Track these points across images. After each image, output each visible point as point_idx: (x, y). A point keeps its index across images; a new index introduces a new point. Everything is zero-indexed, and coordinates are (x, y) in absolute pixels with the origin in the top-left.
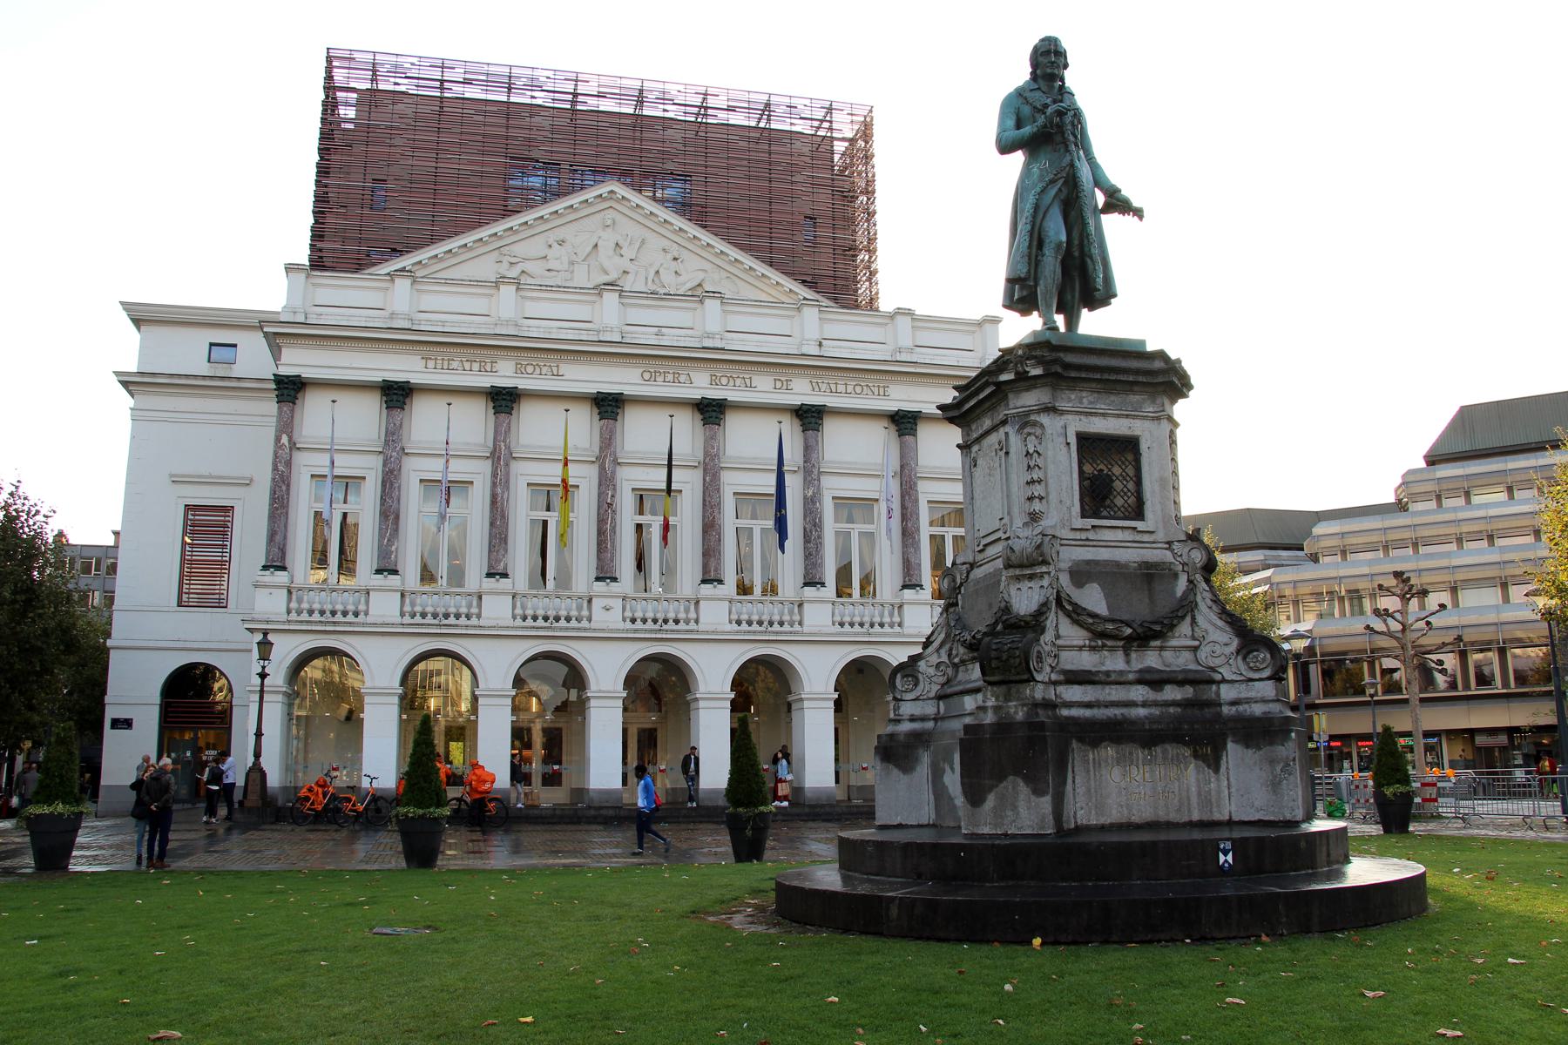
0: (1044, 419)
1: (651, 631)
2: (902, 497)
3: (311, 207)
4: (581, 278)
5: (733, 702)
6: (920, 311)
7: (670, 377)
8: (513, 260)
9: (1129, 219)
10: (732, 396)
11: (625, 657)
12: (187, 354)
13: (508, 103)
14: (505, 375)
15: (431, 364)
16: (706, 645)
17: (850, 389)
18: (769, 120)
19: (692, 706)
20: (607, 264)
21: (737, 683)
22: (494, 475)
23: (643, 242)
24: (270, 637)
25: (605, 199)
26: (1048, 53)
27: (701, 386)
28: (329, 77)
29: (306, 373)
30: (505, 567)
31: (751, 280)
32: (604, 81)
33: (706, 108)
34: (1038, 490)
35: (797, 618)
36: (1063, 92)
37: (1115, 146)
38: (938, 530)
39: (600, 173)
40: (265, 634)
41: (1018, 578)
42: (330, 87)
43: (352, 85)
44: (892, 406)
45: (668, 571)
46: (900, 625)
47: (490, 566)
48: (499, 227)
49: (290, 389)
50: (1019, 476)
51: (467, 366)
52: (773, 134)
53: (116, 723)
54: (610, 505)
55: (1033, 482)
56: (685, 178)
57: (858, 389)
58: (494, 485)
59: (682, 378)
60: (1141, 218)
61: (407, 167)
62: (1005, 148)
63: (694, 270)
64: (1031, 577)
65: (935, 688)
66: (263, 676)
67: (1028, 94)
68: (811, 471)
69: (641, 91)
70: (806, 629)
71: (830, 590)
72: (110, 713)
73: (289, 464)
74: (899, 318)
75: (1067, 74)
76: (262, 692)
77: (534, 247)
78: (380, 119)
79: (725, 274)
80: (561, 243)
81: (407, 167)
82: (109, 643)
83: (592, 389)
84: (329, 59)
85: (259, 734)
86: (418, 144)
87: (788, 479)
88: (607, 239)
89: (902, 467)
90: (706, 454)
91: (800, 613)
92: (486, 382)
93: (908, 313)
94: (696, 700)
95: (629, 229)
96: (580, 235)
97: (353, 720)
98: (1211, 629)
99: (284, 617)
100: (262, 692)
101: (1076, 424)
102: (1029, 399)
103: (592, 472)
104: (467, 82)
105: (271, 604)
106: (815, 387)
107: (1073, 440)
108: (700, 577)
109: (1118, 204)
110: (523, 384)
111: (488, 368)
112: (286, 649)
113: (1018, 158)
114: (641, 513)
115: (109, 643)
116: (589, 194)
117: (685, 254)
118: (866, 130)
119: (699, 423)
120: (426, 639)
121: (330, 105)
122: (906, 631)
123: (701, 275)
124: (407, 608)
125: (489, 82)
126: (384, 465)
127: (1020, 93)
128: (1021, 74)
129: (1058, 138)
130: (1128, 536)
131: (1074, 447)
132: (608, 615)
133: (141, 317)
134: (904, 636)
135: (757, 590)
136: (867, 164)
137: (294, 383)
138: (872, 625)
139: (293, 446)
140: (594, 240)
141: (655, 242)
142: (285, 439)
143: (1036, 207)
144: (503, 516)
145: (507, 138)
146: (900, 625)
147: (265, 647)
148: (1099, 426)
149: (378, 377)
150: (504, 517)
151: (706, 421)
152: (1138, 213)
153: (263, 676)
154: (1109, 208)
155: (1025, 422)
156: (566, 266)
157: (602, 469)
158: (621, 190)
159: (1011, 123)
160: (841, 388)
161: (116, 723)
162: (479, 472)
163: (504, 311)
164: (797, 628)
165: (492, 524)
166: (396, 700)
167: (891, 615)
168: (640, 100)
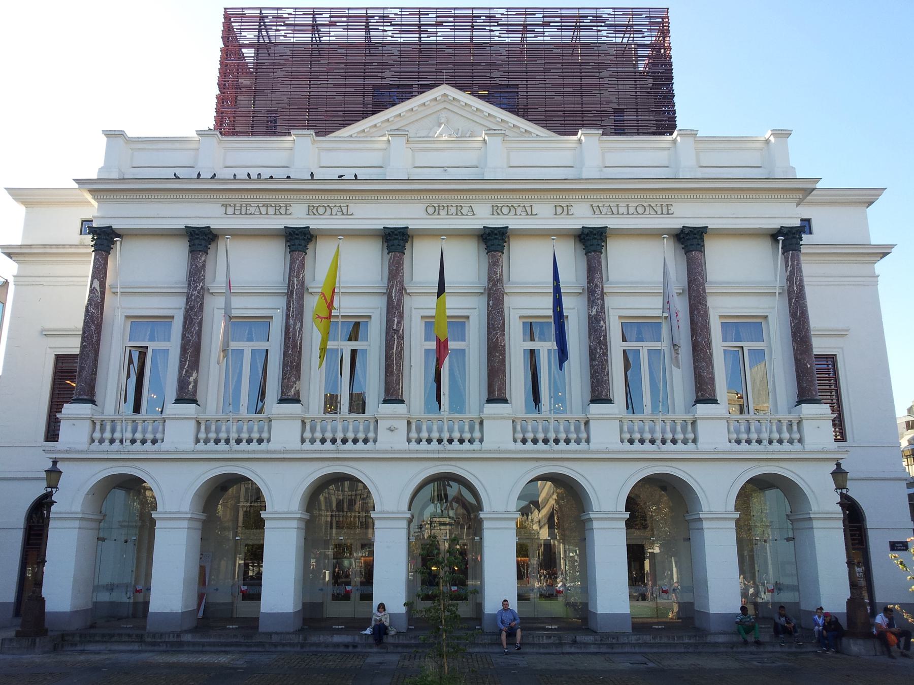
1: (223, 452)
2: (691, 312)
3: (216, 81)
5: (737, 521)
6: (131, 133)
10: (512, 223)
11: (627, 477)
14: (298, 218)
15: (230, 210)
19: (587, 526)
21: (631, 503)
30: (298, 393)
31: (456, 110)
35: (691, 436)
38: (630, 345)
44: (676, 223)
45: (558, 398)
46: (800, 441)
47: (697, 396)
51: (263, 210)
54: (397, 331)
59: (252, 210)
68: (594, 291)
70: (593, 445)
71: (619, 405)
83: (379, 225)
87: (566, 302)
89: (690, 282)
91: (694, 431)
92: (279, 223)
99: (297, 445)
108: (486, 397)
110: (314, 224)
111: (283, 211)
114: (532, 339)
119: (484, 252)
120: (217, 464)
122: (808, 447)
124: (202, 435)
126: (187, 303)
132: (179, 433)
134: (804, 452)
137: (305, 234)
138: (771, 442)
144: (295, 346)
146: (800, 441)
149: (180, 224)
151: (489, 250)
163: (401, 162)
164: (583, 446)
165: (285, 354)
166: (732, 524)
167: (472, 430)
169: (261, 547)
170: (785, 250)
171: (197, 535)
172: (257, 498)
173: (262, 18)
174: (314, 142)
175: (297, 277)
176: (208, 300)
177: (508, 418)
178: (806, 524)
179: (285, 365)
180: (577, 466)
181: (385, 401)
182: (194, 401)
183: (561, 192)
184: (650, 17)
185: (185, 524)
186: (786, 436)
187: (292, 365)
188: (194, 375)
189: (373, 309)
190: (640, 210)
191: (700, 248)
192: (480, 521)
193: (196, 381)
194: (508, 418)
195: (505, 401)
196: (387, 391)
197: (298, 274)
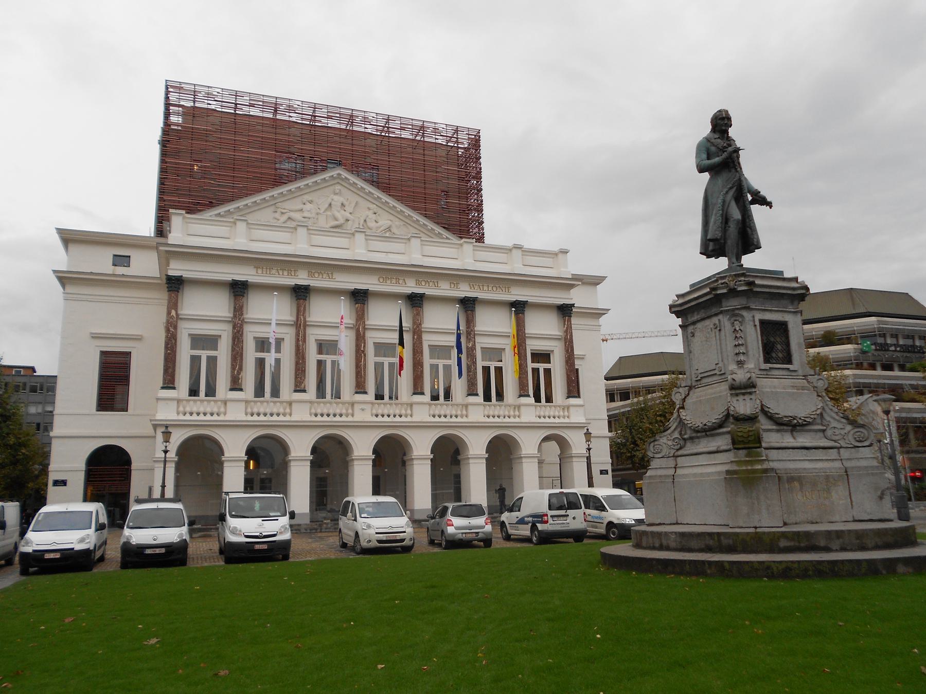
0: (745, 313)
4: (323, 222)
6: (527, 245)
9: (765, 208)
12: (100, 262)
14: (302, 279)
18: (423, 136)
19: (350, 464)
20: (338, 215)
22: (297, 335)
23: (357, 203)
24: (170, 429)
26: (723, 119)
27: (411, 287)
28: (167, 98)
29: (186, 275)
32: (331, 110)
33: (388, 128)
34: (742, 349)
36: (729, 139)
37: (754, 172)
38: (435, 361)
41: (737, 395)
42: (168, 105)
43: (182, 103)
44: (513, 298)
47: (296, 386)
48: (276, 192)
49: (175, 284)
50: (730, 342)
51: (281, 273)
53: (57, 483)
54: (363, 351)
55: (739, 345)
56: (375, 167)
58: (298, 340)
59: (401, 282)
60: (771, 207)
61: (216, 154)
62: (701, 170)
63: (385, 220)
64: (744, 394)
65: (673, 452)
66: (166, 452)
67: (713, 141)
68: (417, 332)
72: (52, 477)
73: (175, 327)
74: (514, 251)
75: (730, 130)
76: (165, 462)
77: (295, 204)
78: (200, 126)
79: (402, 223)
80: (311, 202)
81: (216, 154)
82: (51, 434)
84: (167, 88)
86: (223, 141)
87: (405, 336)
88: (338, 199)
90: (414, 323)
92: (292, 282)
93: (518, 247)
94: (353, 460)
95: (349, 198)
96: (322, 199)
98: (832, 420)
101: (759, 316)
102: (734, 303)
103: (352, 335)
105: (166, 413)
106: (418, 283)
107: (757, 323)
109: (761, 200)
110: (313, 283)
112: (178, 437)
113: (706, 176)
115: (51, 434)
116: (326, 175)
117: (380, 211)
118: (476, 143)
121: (167, 114)
127: (707, 139)
128: (706, 129)
129: (732, 165)
130: (785, 373)
131: (758, 327)
133: (69, 238)
135: (386, 397)
136: (476, 162)
140: (329, 200)
141: (364, 204)
142: (173, 313)
143: (724, 202)
145: (276, 140)
147: (167, 435)
148: (768, 316)
150: (304, 358)
152: (769, 204)
153: (166, 452)
154: (753, 202)
155: (734, 314)
156: (313, 215)
157: (358, 331)
158: (345, 174)
159: (704, 156)
160: (485, 288)
161: (57, 483)
162: (289, 335)
163: (238, 238)
170: (517, 313)
172: (284, 448)
174: (184, 218)
178: (569, 460)
180: (347, 431)
181: (231, 390)
191: (473, 310)
195: (241, 390)
196: (469, 388)
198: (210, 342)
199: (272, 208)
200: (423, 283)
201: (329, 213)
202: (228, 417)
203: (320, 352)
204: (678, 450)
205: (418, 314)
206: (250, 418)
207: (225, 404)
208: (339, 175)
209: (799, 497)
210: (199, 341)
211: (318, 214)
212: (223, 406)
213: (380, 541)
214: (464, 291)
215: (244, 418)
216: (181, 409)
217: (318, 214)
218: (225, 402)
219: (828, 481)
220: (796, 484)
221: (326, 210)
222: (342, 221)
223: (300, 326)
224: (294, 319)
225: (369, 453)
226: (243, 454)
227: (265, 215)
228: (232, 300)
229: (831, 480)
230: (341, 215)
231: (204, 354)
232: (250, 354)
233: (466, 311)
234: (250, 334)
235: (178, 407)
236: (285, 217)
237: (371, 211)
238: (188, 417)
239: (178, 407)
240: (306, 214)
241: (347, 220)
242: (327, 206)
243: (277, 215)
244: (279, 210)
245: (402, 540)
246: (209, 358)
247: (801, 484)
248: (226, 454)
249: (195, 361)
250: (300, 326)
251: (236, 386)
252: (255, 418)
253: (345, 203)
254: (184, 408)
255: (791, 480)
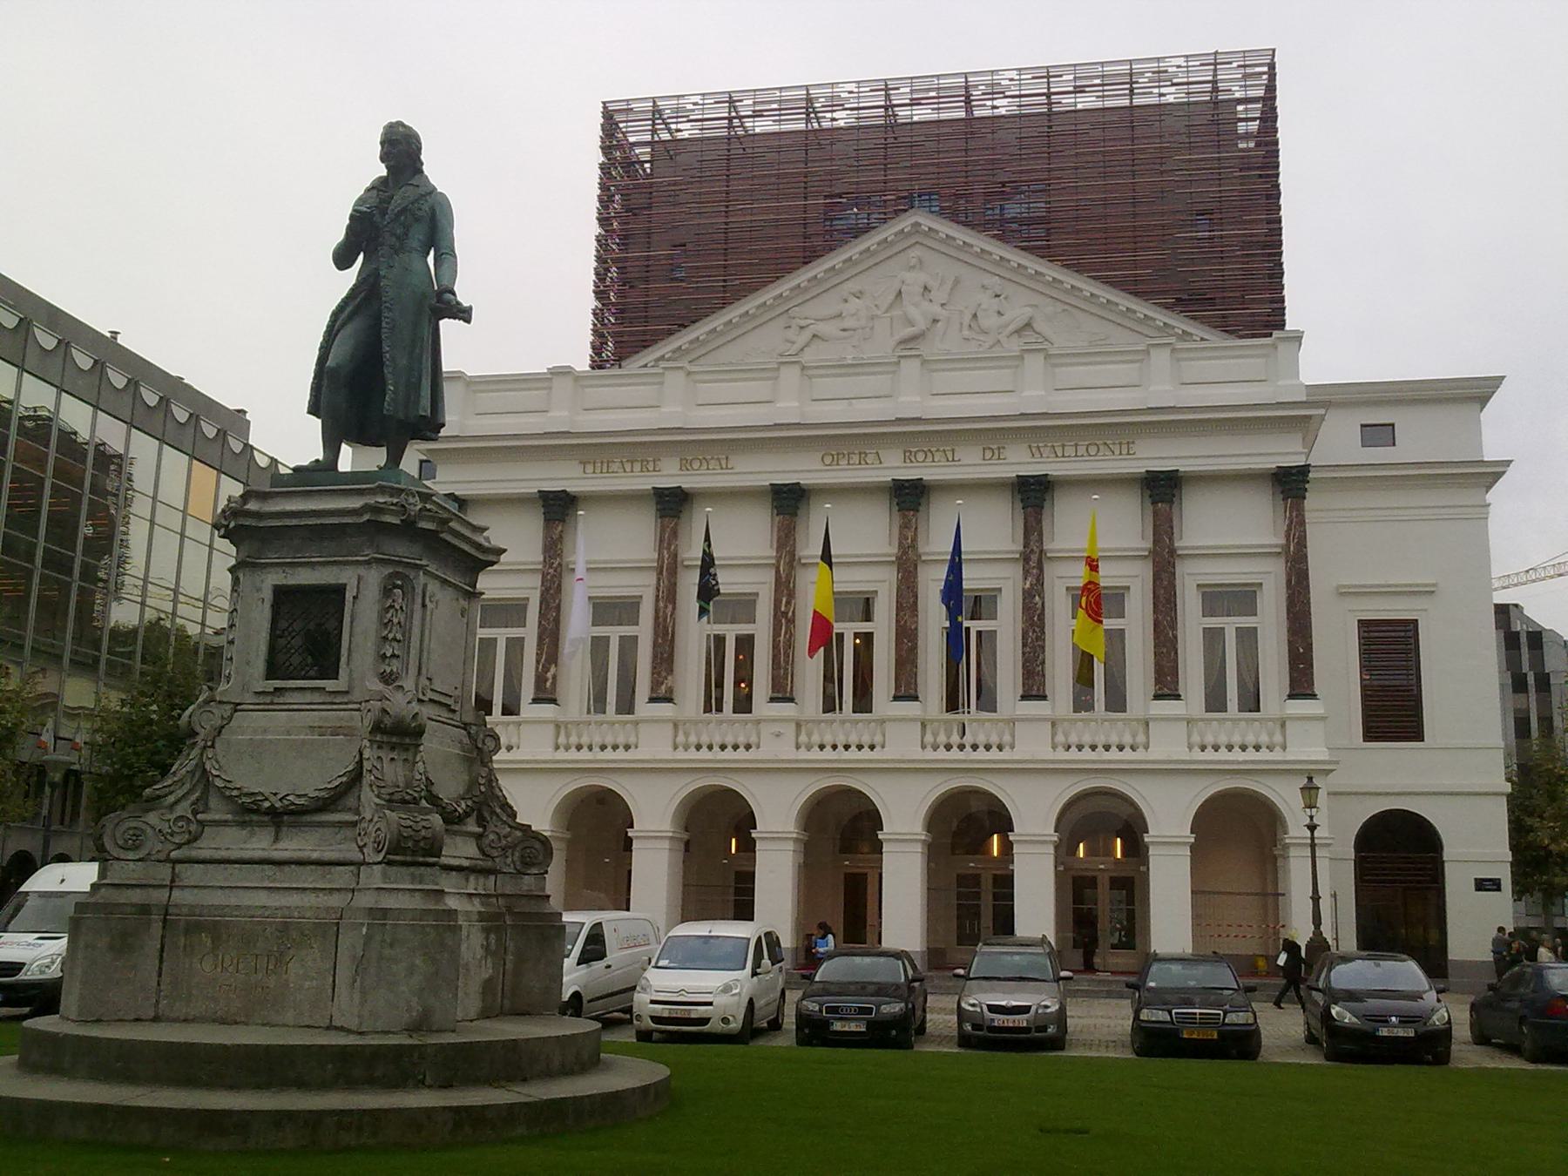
7: (856, 459)
8: (803, 323)
13: (1132, 107)
14: (670, 476)
15: (590, 468)
16: (1477, 790)
17: (1082, 450)
20: (914, 313)
23: (957, 282)
25: (910, 234)
27: (893, 467)
30: (670, 690)
39: (907, 202)
40: (1310, 779)
47: (897, 688)
51: (628, 467)
52: (1137, 113)
53: (1495, 885)
54: (785, 614)
57: (1093, 450)
66: (1312, 828)
69: (967, 88)
74: (558, 383)
76: (1313, 846)
77: (828, 305)
80: (859, 295)
85: (1316, 898)
88: (915, 279)
92: (646, 483)
97: (385, 912)
100: (1313, 846)
104: (1079, 90)
110: (687, 482)
123: (1028, 311)
125: (942, 96)
138: (835, 747)
139: (1172, 552)
153: (1312, 828)
160: (1070, 451)
161: (1495, 885)
168: (1131, 81)
169: (751, 877)
171: (680, 856)
172: (1000, 820)
173: (657, 112)
175: (669, 549)
176: (567, 582)
177: (1045, 720)
179: (655, 656)
182: (554, 701)
183: (992, 434)
184: (1245, 66)
185: (666, 844)
186: (955, 739)
187: (664, 658)
188: (553, 669)
189: (762, 585)
190: (1093, 450)
192: (880, 843)
193: (554, 677)
194: (1045, 720)
195: (1044, 698)
196: (1293, 682)
197: (669, 545)
198: (1241, 599)
199: (782, 322)
200: (921, 456)
201: (896, 312)
202: (1017, 755)
203: (1208, 611)
204: (179, 846)
205: (675, 534)
206: (1198, 755)
207: (1283, 725)
208: (917, 224)
209: (207, 966)
210: (1223, 599)
211: (873, 318)
212: (1141, 729)
213: (657, 1019)
214: (1021, 462)
215: (1049, 754)
216: (1060, 738)
217: (873, 318)
218: (1012, 722)
219: (287, 935)
220: (206, 939)
221: (891, 306)
222: (922, 325)
223: (1164, 560)
224: (1149, 545)
225: (1185, 833)
226: (1052, 831)
227: (766, 342)
228: (897, 521)
229: (294, 934)
230: (920, 313)
231: (1230, 625)
232: (1192, 622)
233: (1154, 503)
234: (1189, 580)
235: (798, 736)
236: (807, 334)
237: (989, 292)
238: (816, 754)
239: (1054, 735)
240: (847, 324)
241: (935, 321)
242: (891, 297)
243: (791, 334)
244: (794, 323)
245: (704, 1021)
246: (739, 639)
247: (216, 940)
248: (1151, 832)
249: (1213, 638)
250: (1164, 560)
251: (1166, 687)
252: (1209, 755)
253: (932, 284)
254: (1066, 735)
255: (193, 928)
